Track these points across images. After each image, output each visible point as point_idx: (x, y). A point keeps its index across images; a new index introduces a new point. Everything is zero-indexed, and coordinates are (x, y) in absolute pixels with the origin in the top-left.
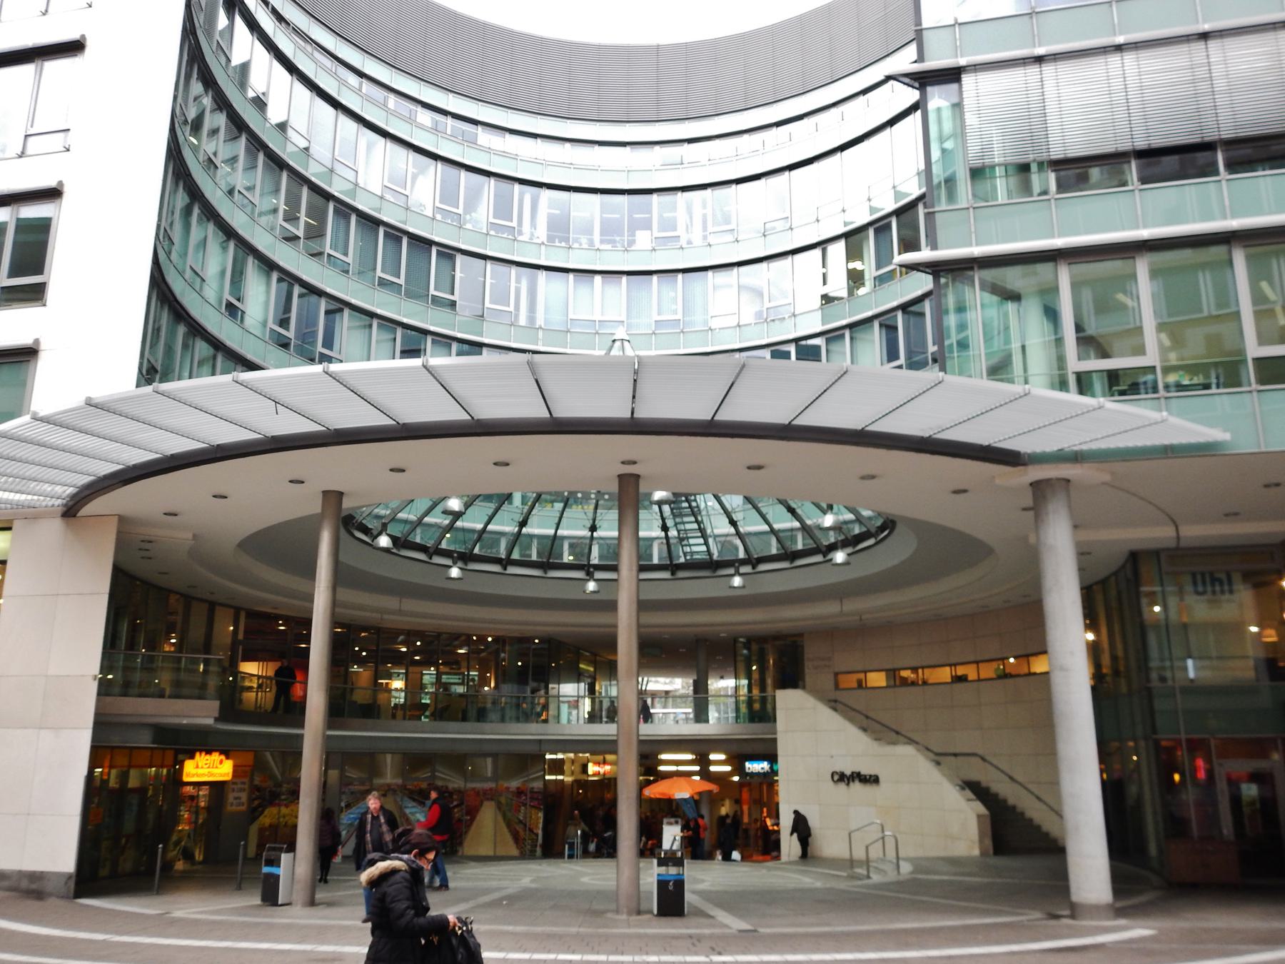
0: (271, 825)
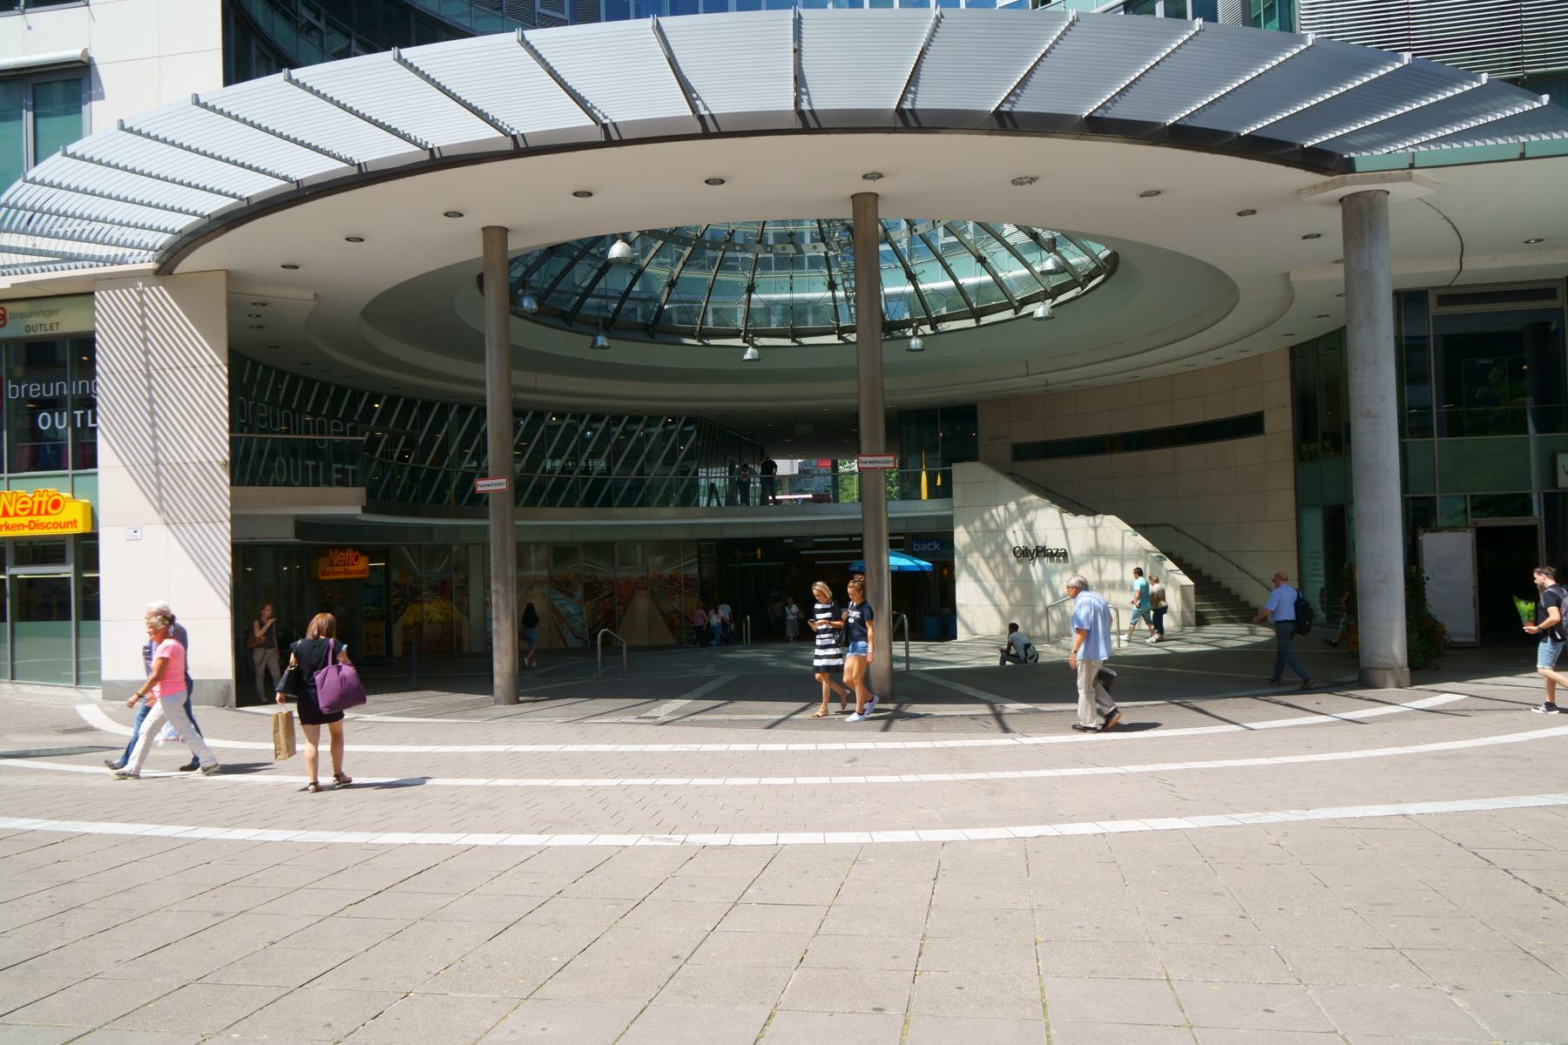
0: (414, 623)
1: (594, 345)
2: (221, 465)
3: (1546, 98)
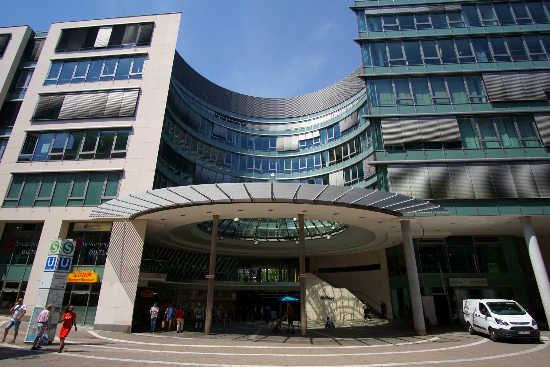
1: (220, 239)
2: (138, 267)
3: (439, 206)
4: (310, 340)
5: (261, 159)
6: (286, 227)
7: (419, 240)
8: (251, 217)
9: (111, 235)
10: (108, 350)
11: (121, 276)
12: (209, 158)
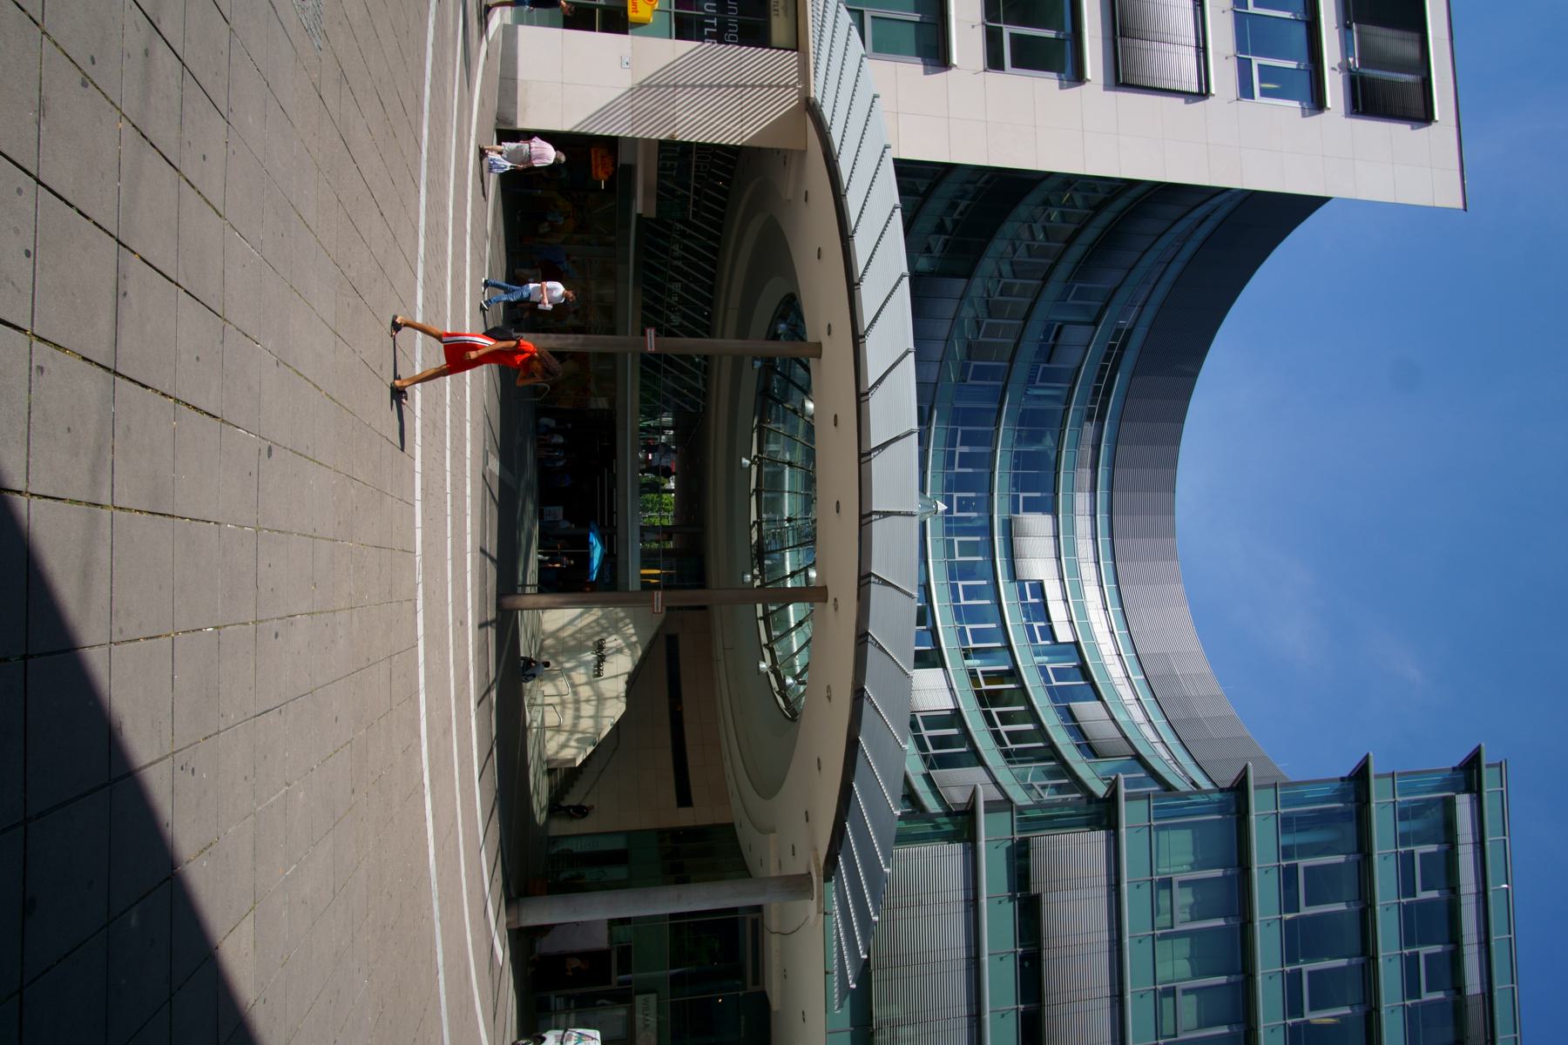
1: (755, 358)
2: (672, 135)
3: (854, 986)
4: (489, 619)
5: (986, 471)
6: (791, 544)
7: (757, 920)
8: (817, 446)
9: (760, 49)
10: (450, 74)
11: (645, 89)
12: (990, 316)
